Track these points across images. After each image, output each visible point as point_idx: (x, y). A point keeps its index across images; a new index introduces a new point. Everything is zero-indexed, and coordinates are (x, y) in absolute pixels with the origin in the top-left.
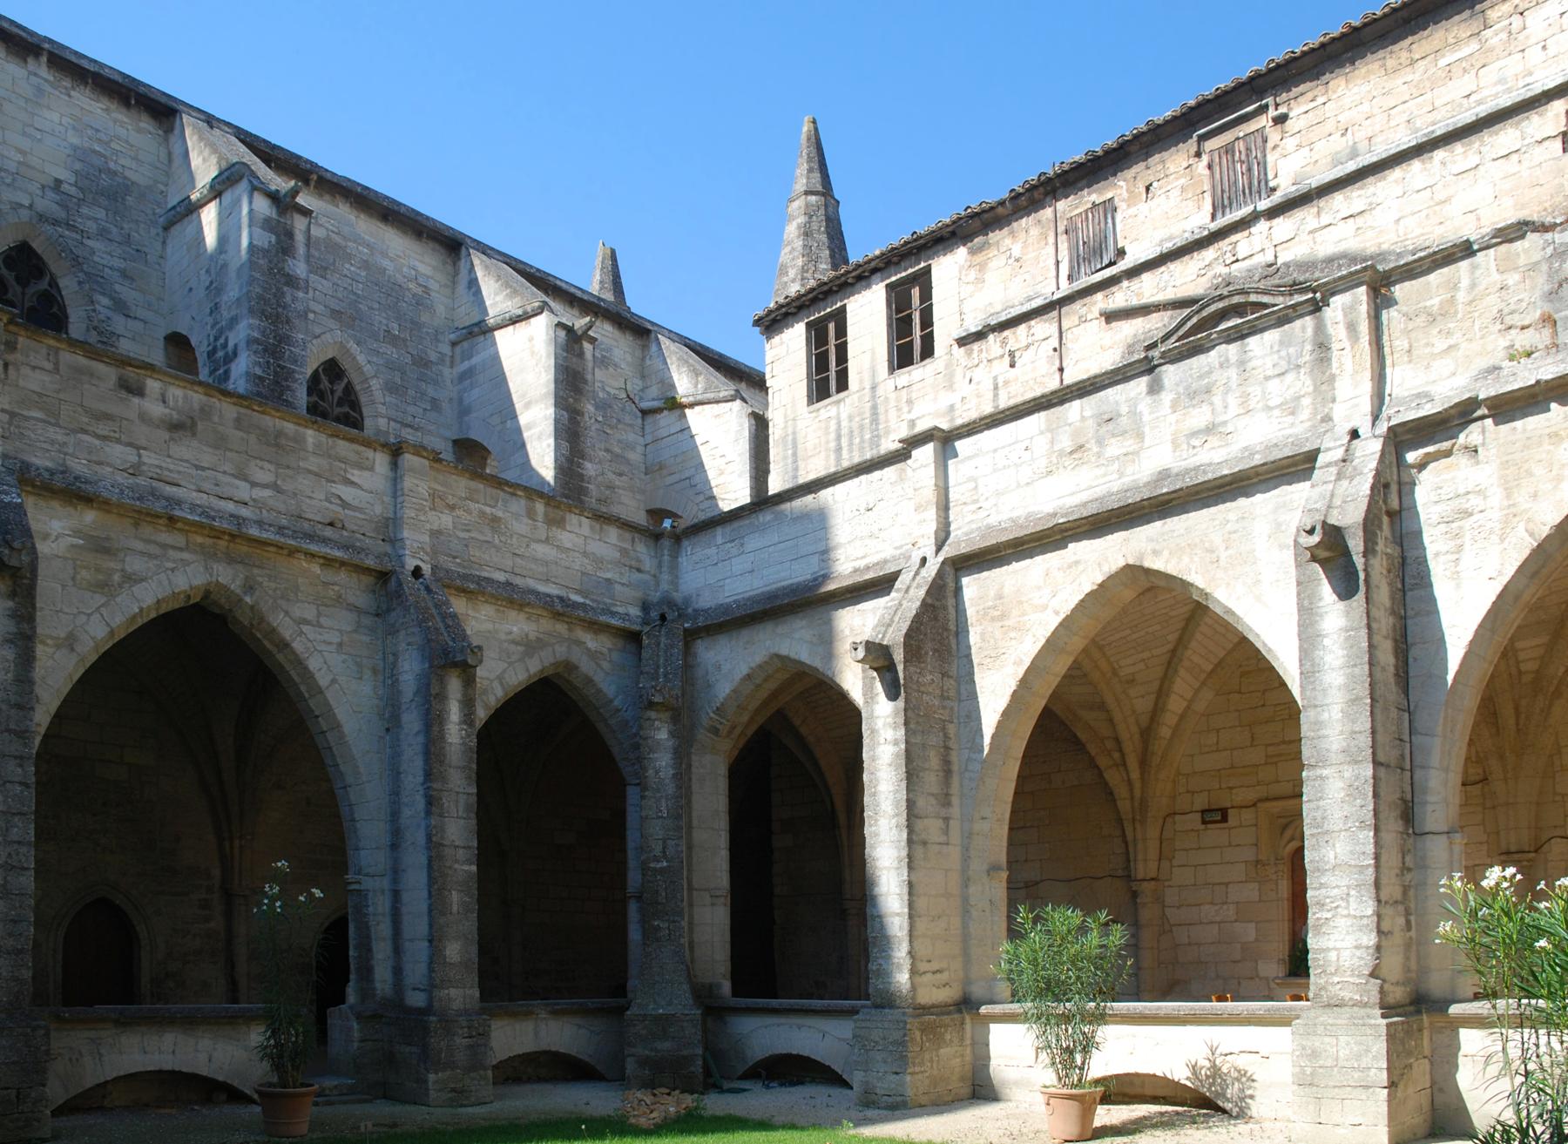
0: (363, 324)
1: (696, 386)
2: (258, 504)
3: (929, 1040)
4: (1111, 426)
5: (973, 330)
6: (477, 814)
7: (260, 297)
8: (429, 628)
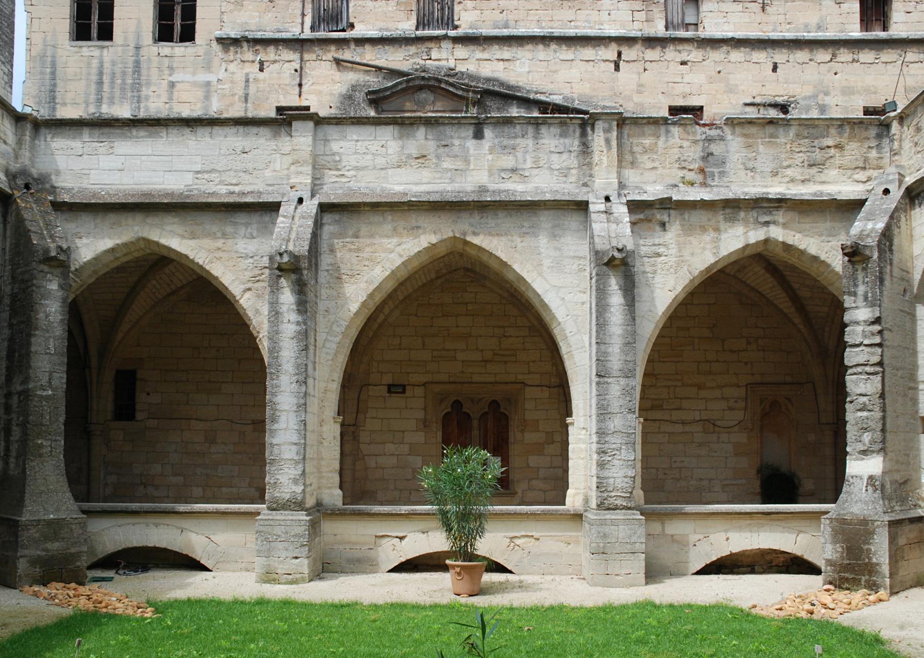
4: (446, 149)
5: (233, 36)
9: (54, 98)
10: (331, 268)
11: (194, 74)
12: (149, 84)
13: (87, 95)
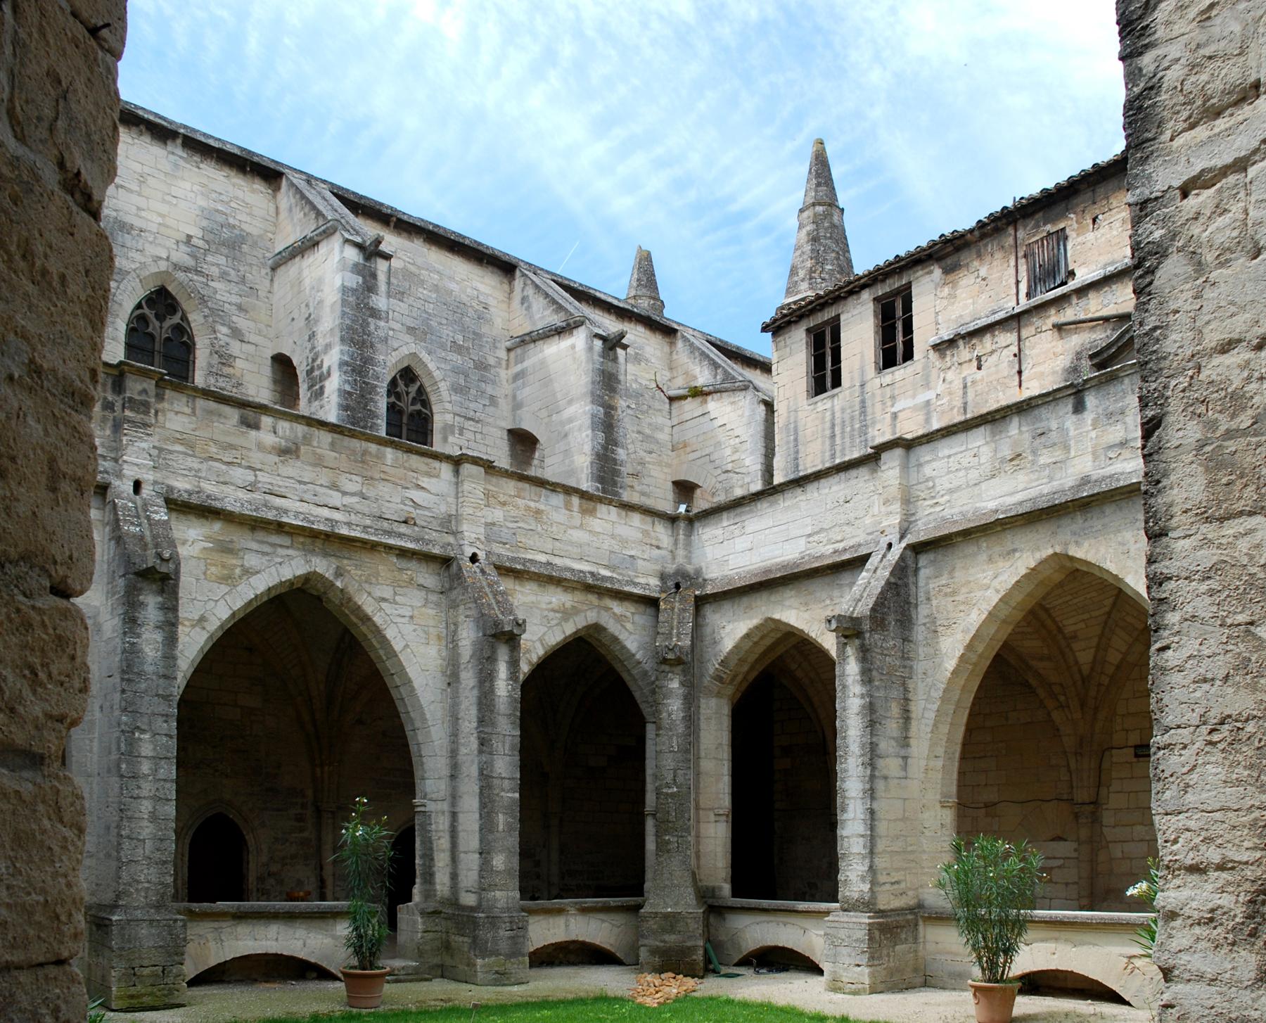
0: (434, 338)
1: (715, 377)
2: (348, 509)
3: (887, 939)
4: (1043, 439)
5: (946, 338)
6: (520, 751)
7: (349, 328)
8: (483, 604)
10: (927, 620)
11: (914, 396)
12: (874, 423)
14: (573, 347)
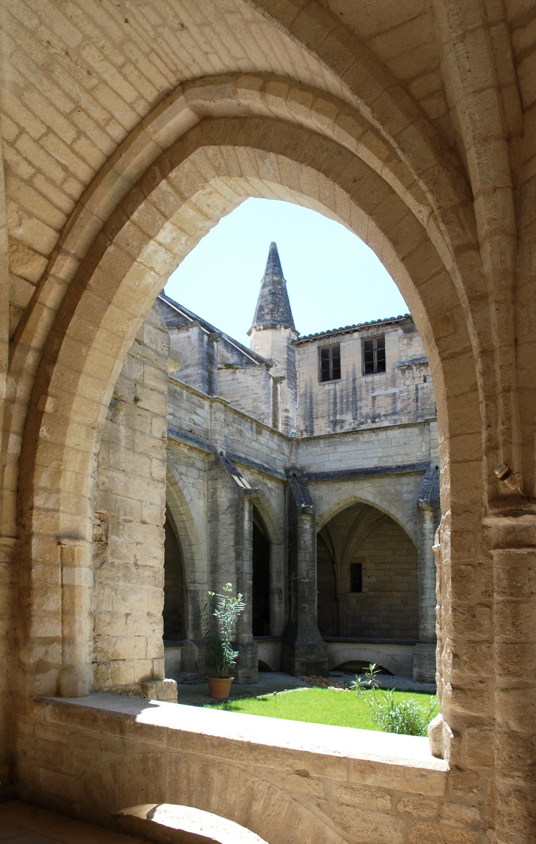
9: (312, 415)
11: (386, 390)
12: (361, 399)
13: (329, 410)
14: (189, 337)
